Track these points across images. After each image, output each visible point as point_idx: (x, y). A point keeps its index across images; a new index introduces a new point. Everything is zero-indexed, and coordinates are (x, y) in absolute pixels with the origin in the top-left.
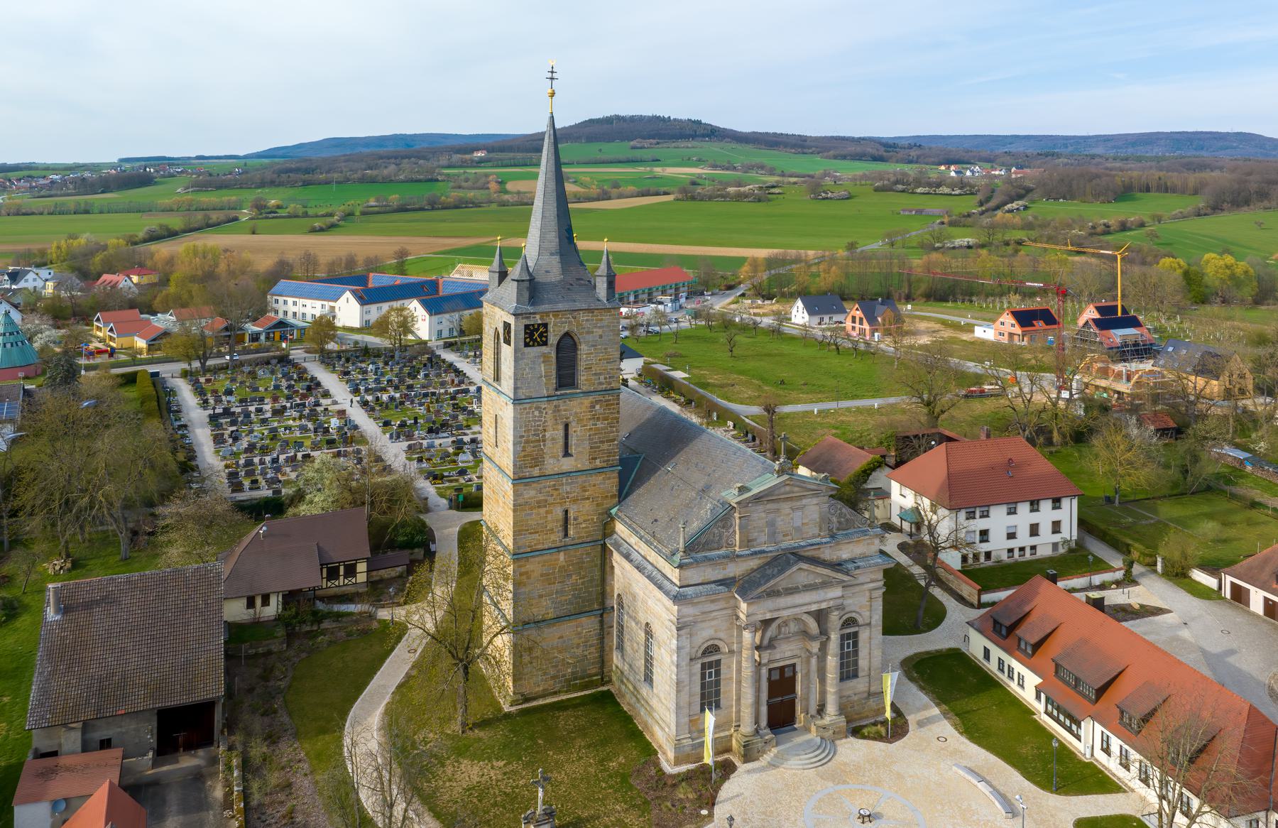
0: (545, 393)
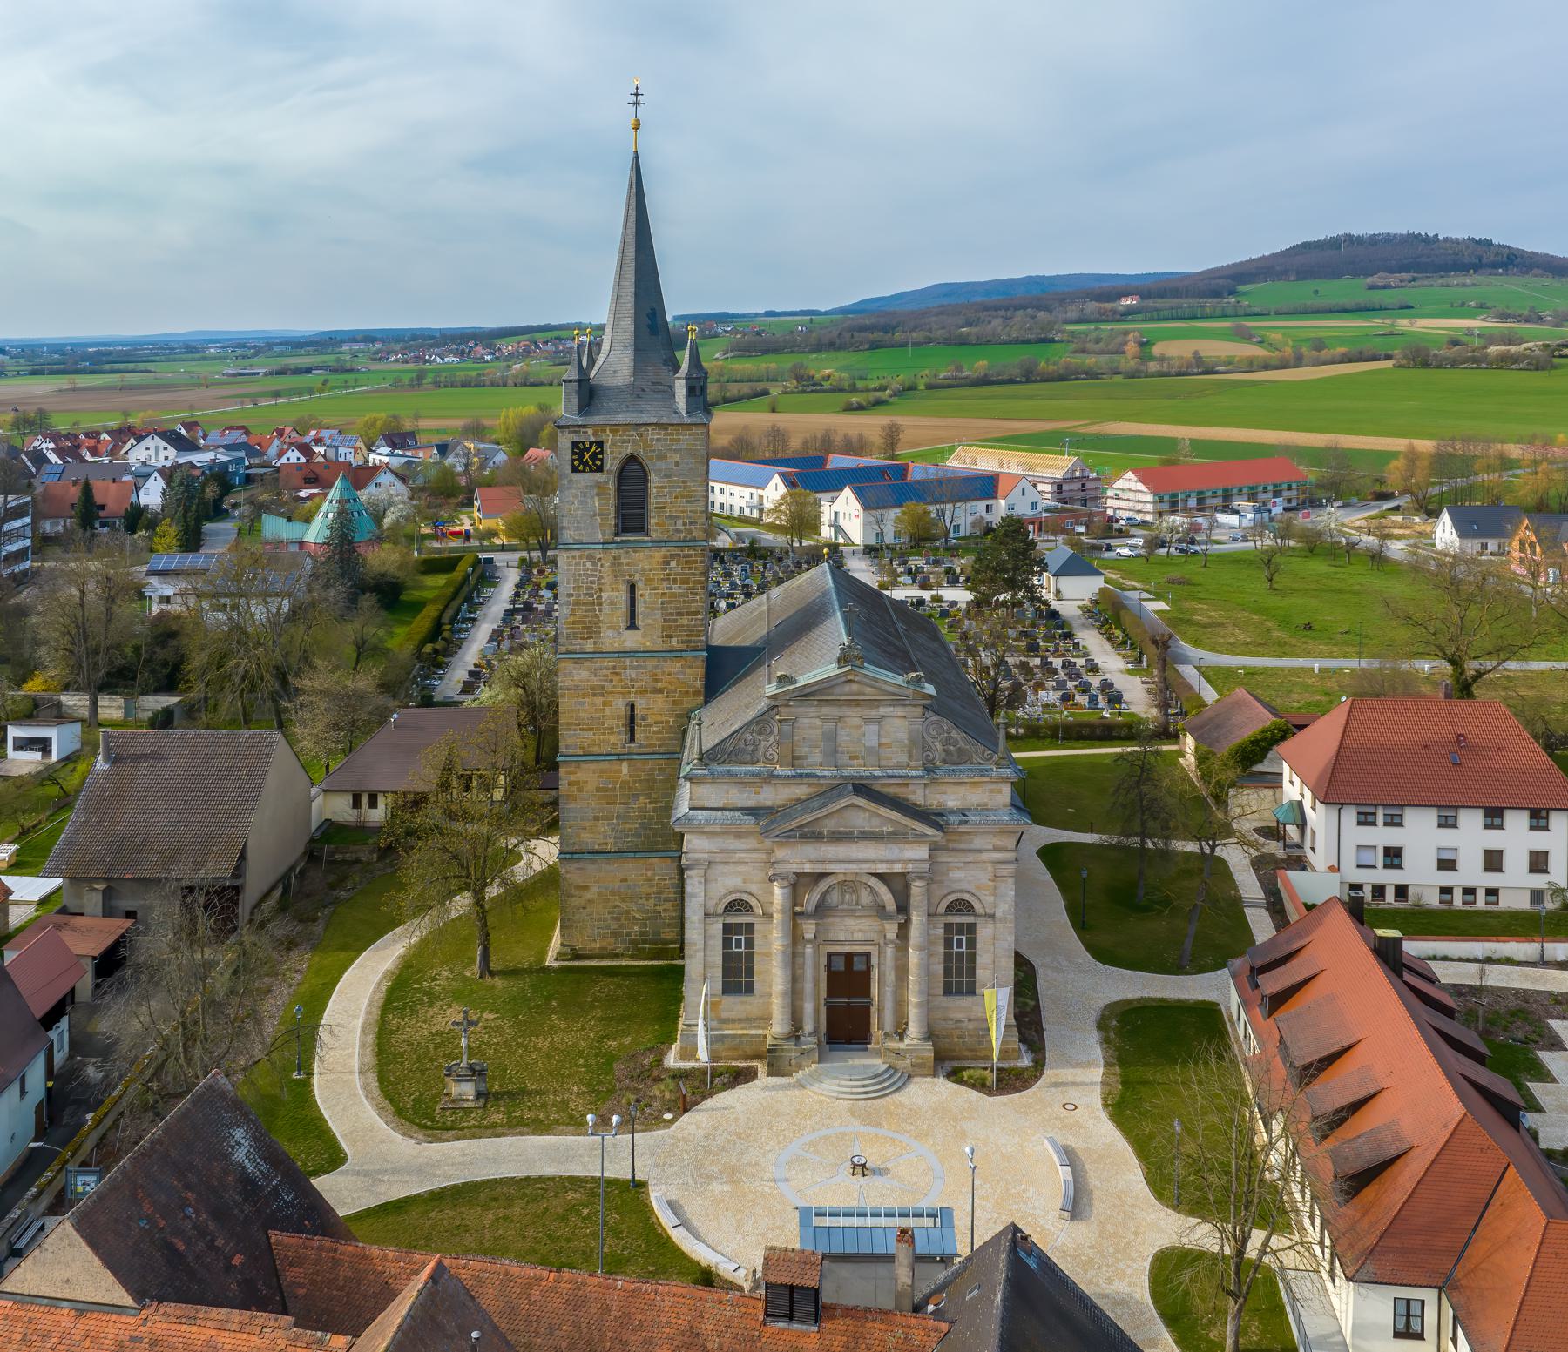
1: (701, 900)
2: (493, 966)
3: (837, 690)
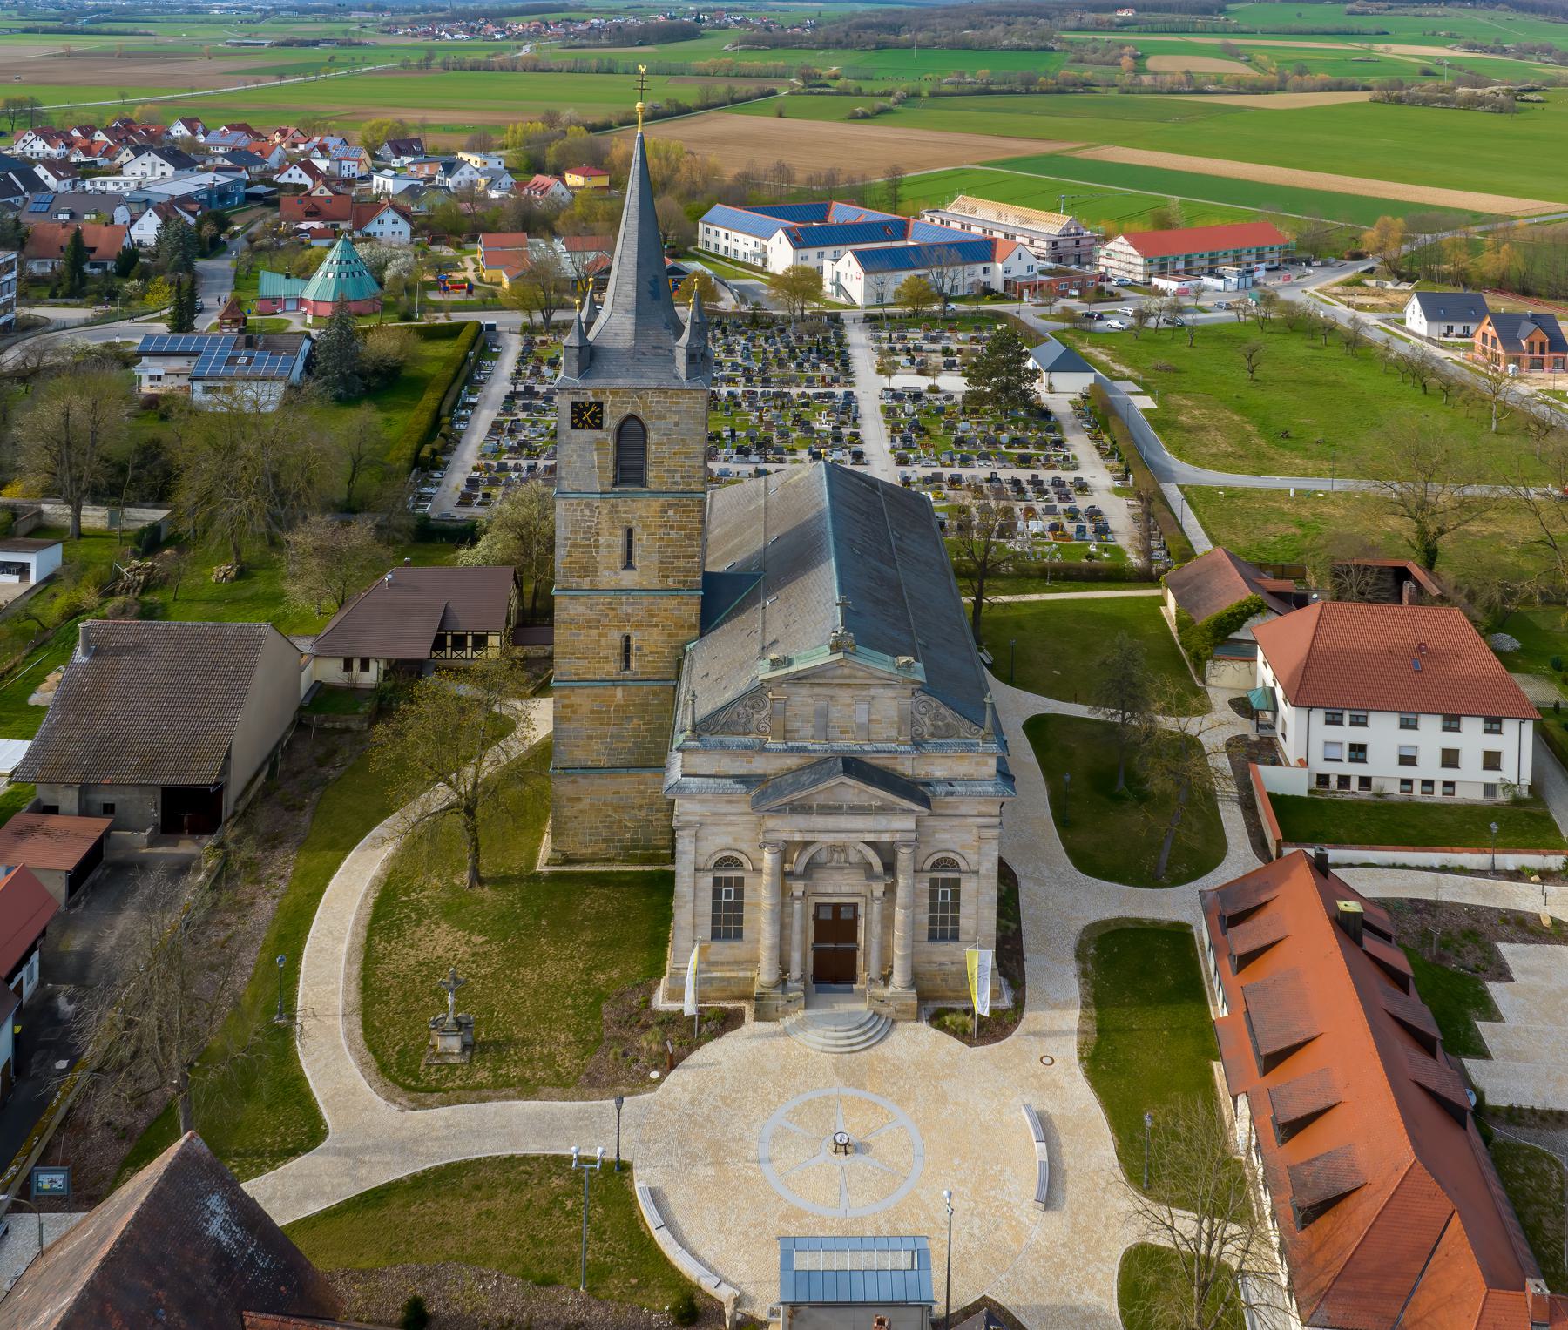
0: (598, 488)
1: (692, 857)
2: (484, 873)
3: (829, 674)
